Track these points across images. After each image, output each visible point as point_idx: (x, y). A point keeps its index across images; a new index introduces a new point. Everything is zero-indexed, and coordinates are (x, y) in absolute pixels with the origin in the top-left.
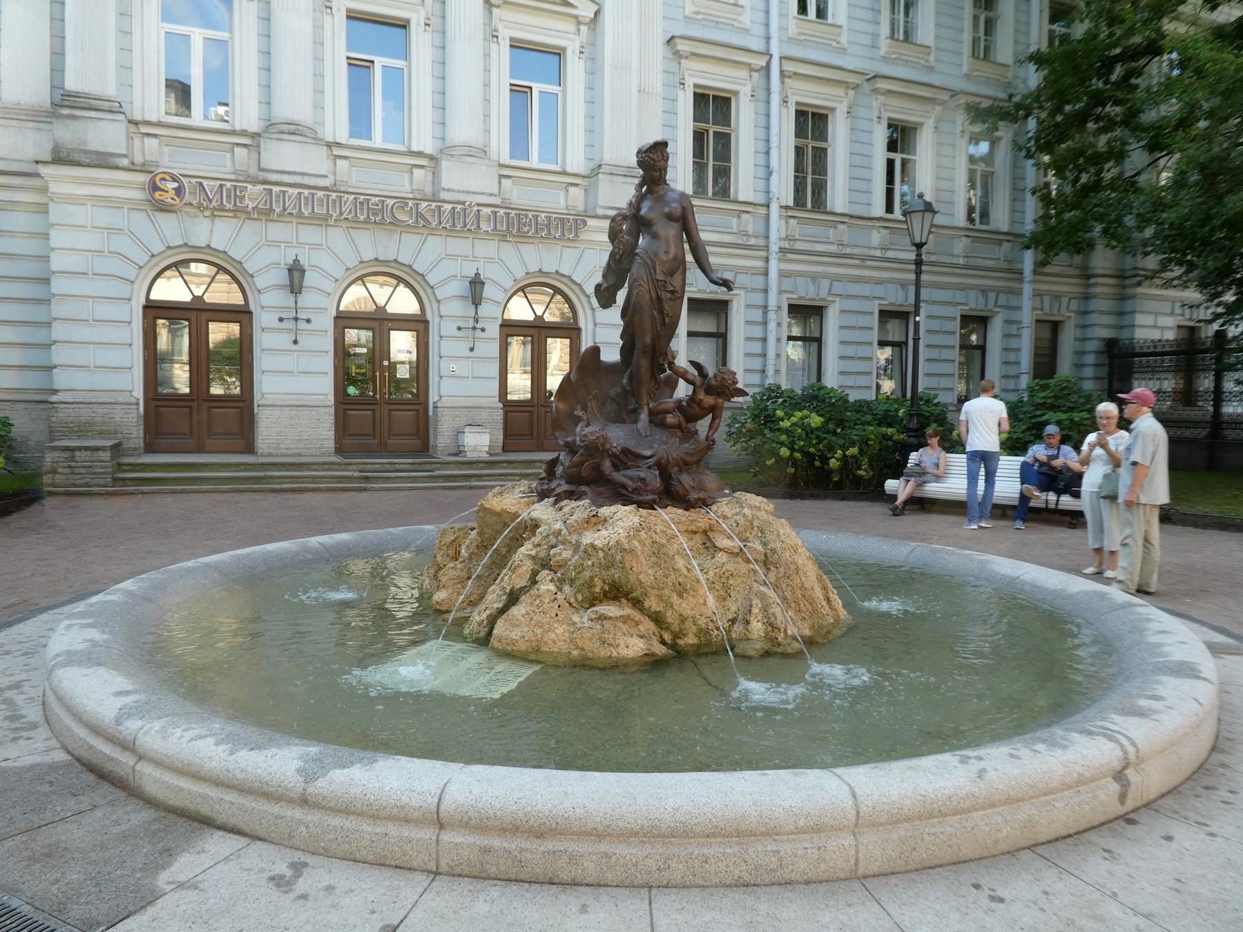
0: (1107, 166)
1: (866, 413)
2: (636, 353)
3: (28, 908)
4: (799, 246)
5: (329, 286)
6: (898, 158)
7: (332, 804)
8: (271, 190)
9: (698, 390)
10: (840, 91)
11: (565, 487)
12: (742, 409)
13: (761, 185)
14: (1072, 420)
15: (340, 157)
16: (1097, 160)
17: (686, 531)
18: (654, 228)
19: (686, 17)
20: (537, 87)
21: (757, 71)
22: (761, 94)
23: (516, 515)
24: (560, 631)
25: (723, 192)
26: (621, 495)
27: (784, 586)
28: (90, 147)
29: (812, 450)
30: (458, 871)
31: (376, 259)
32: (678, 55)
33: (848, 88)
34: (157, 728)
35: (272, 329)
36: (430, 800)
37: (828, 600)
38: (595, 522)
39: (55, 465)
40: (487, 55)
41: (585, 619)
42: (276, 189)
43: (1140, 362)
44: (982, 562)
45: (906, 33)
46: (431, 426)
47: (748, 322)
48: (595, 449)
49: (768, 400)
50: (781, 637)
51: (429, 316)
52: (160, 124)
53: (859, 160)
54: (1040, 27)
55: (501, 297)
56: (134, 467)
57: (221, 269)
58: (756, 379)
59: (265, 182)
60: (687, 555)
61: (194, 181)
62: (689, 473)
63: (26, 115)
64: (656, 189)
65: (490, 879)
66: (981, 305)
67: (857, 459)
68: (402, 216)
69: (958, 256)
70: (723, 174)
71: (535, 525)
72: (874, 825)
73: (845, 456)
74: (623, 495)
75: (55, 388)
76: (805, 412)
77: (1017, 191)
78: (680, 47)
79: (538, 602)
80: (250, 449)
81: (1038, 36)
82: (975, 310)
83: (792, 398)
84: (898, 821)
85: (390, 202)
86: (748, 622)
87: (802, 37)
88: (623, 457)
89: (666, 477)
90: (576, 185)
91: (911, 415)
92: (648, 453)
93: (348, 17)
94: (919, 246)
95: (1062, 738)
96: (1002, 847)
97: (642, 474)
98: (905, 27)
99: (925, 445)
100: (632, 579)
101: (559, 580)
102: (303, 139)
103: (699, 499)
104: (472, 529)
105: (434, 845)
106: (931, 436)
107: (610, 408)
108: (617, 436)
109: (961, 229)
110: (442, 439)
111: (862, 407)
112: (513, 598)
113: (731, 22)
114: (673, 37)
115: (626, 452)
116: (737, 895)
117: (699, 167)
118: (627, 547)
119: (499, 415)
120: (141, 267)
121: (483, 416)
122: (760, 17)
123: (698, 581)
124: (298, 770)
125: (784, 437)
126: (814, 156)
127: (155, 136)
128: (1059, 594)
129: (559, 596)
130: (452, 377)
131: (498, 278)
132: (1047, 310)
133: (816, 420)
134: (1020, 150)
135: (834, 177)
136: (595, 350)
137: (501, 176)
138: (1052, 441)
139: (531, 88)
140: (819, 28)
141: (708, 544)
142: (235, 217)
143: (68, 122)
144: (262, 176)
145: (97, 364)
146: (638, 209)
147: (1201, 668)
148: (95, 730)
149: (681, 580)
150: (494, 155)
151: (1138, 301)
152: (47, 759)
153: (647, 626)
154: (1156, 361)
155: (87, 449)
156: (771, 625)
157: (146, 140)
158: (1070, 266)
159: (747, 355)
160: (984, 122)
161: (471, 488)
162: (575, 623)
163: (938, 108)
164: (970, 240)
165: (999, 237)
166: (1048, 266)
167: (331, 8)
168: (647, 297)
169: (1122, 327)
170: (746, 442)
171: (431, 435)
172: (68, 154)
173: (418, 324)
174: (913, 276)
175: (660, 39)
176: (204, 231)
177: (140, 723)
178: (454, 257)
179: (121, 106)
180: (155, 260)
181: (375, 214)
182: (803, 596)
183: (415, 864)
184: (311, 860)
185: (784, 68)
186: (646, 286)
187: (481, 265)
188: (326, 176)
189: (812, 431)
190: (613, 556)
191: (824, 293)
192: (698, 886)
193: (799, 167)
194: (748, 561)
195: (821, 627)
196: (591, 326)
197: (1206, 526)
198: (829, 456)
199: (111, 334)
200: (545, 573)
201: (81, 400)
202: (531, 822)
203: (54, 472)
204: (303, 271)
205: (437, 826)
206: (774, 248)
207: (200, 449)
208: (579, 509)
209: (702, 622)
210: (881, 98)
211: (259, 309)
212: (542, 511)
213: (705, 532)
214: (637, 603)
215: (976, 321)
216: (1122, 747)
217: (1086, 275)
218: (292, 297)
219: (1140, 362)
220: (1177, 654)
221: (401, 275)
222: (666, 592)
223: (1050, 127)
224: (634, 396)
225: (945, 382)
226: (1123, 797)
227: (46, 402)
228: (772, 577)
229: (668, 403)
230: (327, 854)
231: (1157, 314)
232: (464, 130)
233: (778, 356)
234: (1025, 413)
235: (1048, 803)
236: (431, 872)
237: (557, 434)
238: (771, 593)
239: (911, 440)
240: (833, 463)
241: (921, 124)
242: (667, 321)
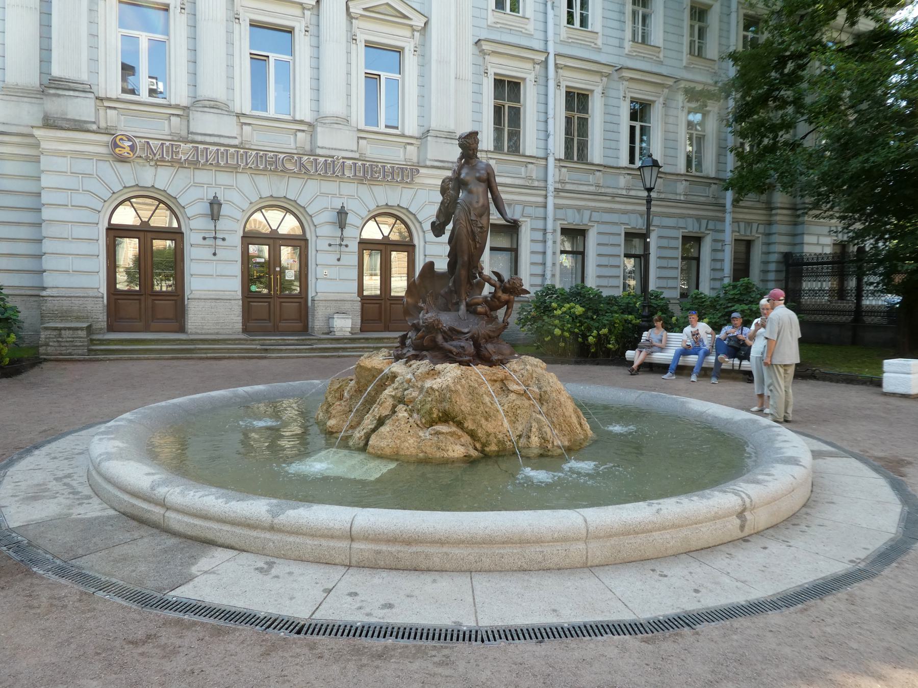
0: (780, 134)
1: (613, 305)
2: (458, 267)
3: (122, 582)
4: (568, 187)
5: (238, 215)
6: (638, 125)
7: (289, 529)
8: (197, 147)
9: (498, 290)
10: (597, 78)
11: (413, 352)
12: (529, 302)
13: (542, 144)
14: (751, 310)
15: (246, 124)
16: (774, 129)
17: (490, 380)
18: (469, 187)
19: (488, 26)
20: (384, 75)
21: (539, 64)
22: (541, 80)
23: (381, 371)
24: (411, 441)
25: (515, 148)
26: (449, 357)
27: (552, 414)
28: (69, 117)
29: (576, 330)
30: (362, 564)
31: (271, 196)
32: (483, 52)
33: (602, 76)
34: (178, 491)
35: (198, 245)
36: (346, 525)
37: (581, 424)
38: (433, 374)
39: (47, 340)
40: (349, 53)
41: (427, 434)
42: (201, 147)
43: (807, 269)
44: (683, 403)
45: (643, 37)
46: (310, 314)
47: (532, 241)
48: (433, 328)
49: (546, 295)
50: (550, 446)
51: (308, 236)
52: (118, 100)
53: (610, 127)
54: (737, 34)
55: (359, 223)
56: (102, 342)
57: (161, 201)
58: (538, 281)
59: (193, 142)
60: (491, 395)
61: (143, 140)
62: (492, 343)
63: (22, 92)
64: (471, 161)
65: (381, 568)
66: (696, 229)
67: (607, 337)
68: (289, 166)
69: (680, 195)
70: (515, 135)
71: (394, 376)
72: (597, 537)
73: (599, 334)
74: (450, 357)
75: (45, 286)
76: (572, 304)
77: (722, 150)
78: (484, 47)
79: (397, 424)
80: (182, 329)
81: (735, 43)
82: (692, 232)
83: (562, 295)
84: (610, 536)
85: (281, 156)
86: (529, 437)
87: (570, 40)
88: (449, 333)
89: (477, 345)
90: (412, 144)
91: (644, 307)
92: (466, 330)
93: (251, 25)
94: (649, 190)
95: (708, 494)
96: (670, 552)
97: (462, 344)
98: (643, 33)
99: (652, 327)
100: (457, 409)
101: (410, 410)
102: (219, 111)
103: (499, 360)
104: (351, 380)
105: (348, 550)
106: (657, 321)
107: (441, 301)
108: (447, 320)
109: (682, 175)
110: (318, 322)
111: (611, 300)
112: (381, 422)
113: (520, 29)
114: (479, 40)
115: (452, 330)
116: (520, 575)
117: (498, 130)
118: (453, 389)
119: (358, 306)
120: (105, 201)
121: (347, 306)
122: (541, 26)
123: (498, 411)
124: (268, 511)
125: (557, 322)
126: (579, 124)
127: (115, 108)
128: (728, 422)
129: (410, 420)
130: (325, 279)
131: (356, 210)
132: (742, 232)
133: (579, 310)
134: (722, 120)
135: (593, 139)
136: (430, 266)
137: (359, 138)
138: (736, 322)
139: (379, 75)
140: (581, 34)
141: (504, 388)
142: (172, 166)
143: (54, 99)
144: (191, 137)
145: (74, 269)
146: (459, 174)
147: (801, 460)
148: (135, 494)
149: (487, 410)
150: (354, 123)
151: (806, 226)
152: (105, 513)
153: (466, 439)
154: (817, 268)
155: (70, 329)
156: (544, 439)
157: (108, 111)
158: (759, 201)
159: (532, 264)
160: (697, 101)
161: (339, 357)
162: (420, 437)
163: (666, 91)
164: (688, 183)
165: (708, 181)
166: (741, 202)
167: (239, 19)
168: (465, 230)
169: (795, 245)
170: (531, 325)
171: (310, 320)
172: (54, 121)
173: (300, 243)
174: (644, 208)
175: (471, 41)
176: (150, 176)
177: (167, 489)
178: (326, 195)
179: (91, 88)
180: (115, 196)
181: (271, 165)
182: (564, 421)
183: (337, 561)
184: (275, 560)
185: (557, 62)
186: (464, 223)
187: (345, 200)
188: (236, 138)
189: (577, 317)
190: (444, 395)
191: (586, 221)
192: (498, 571)
193: (568, 131)
194: (529, 399)
195: (575, 441)
196: (422, 243)
197: (837, 381)
198: (588, 334)
199: (84, 248)
200: (401, 406)
201: (63, 295)
202: (404, 536)
203: (47, 345)
204: (220, 204)
205: (350, 540)
206: (551, 188)
207: (147, 329)
208: (423, 366)
209: (500, 436)
210: (625, 83)
211: (188, 232)
212: (398, 367)
213: (502, 381)
214: (460, 424)
215: (692, 241)
216: (742, 499)
217: (770, 207)
218: (212, 223)
219: (807, 269)
220: (789, 453)
221: (287, 206)
222: (478, 417)
223: (742, 105)
224: (456, 293)
225: (671, 283)
226: (742, 527)
227: (39, 296)
228: (544, 409)
229: (478, 298)
230: (285, 557)
231: (818, 235)
232: (333, 106)
233: (554, 264)
234: (721, 305)
235: (697, 529)
236: (346, 566)
237: (407, 319)
238: (543, 419)
239: (644, 323)
240: (591, 339)
241: (654, 102)
242: (478, 246)
